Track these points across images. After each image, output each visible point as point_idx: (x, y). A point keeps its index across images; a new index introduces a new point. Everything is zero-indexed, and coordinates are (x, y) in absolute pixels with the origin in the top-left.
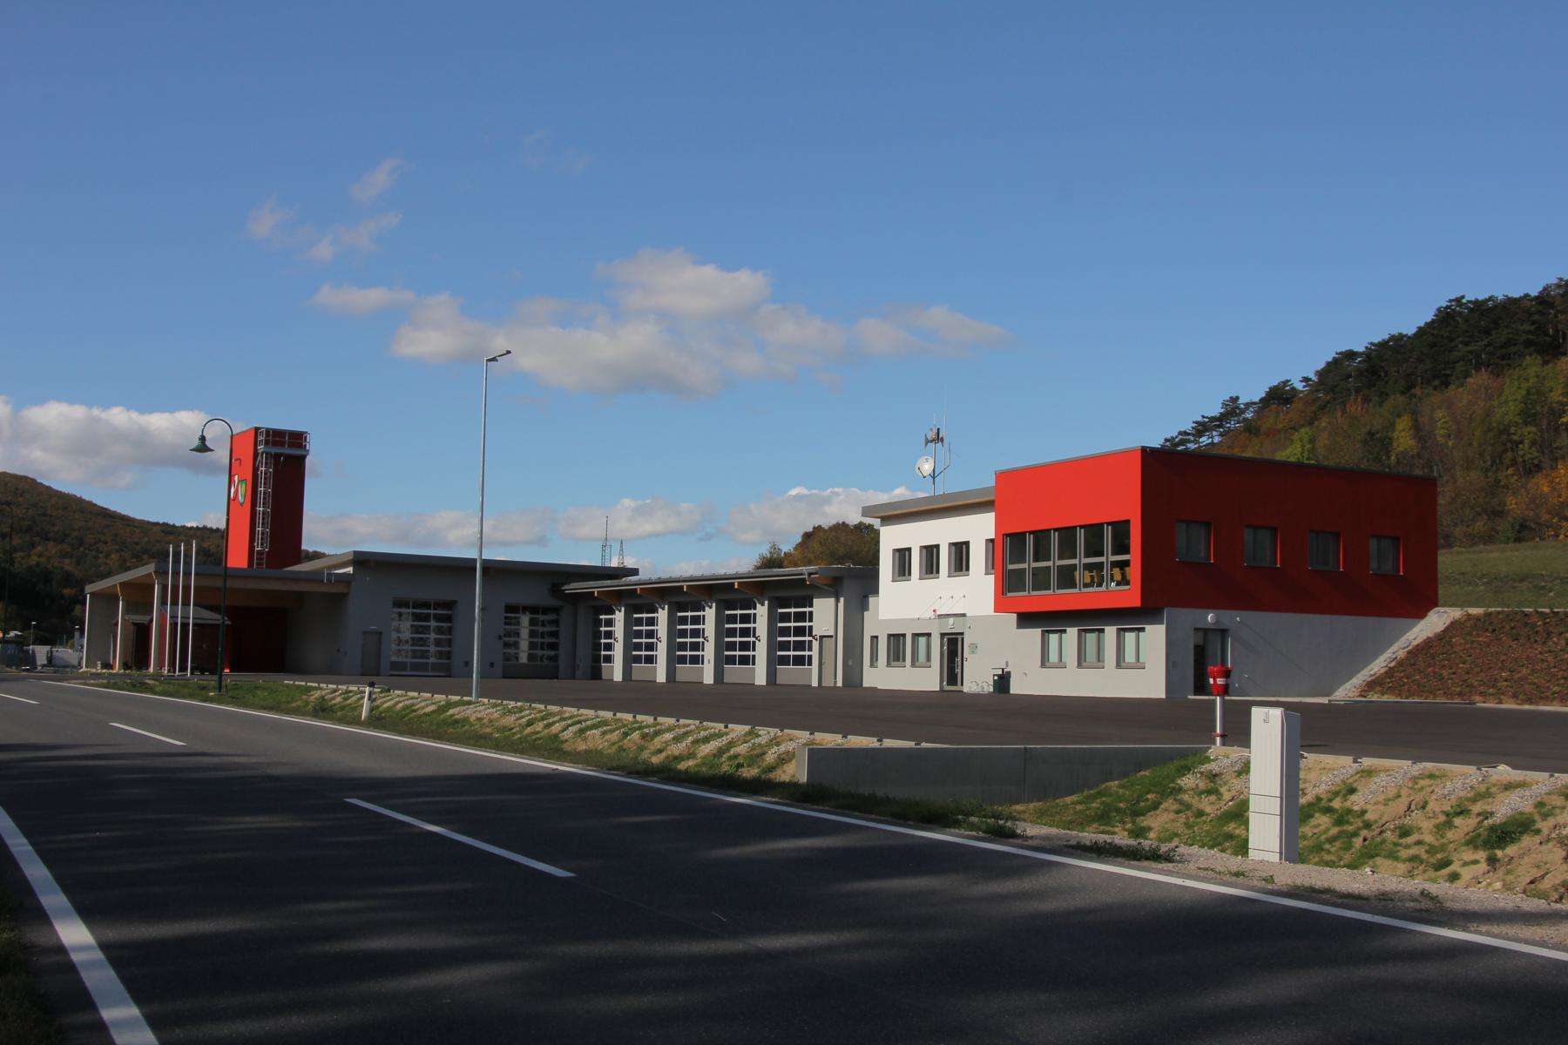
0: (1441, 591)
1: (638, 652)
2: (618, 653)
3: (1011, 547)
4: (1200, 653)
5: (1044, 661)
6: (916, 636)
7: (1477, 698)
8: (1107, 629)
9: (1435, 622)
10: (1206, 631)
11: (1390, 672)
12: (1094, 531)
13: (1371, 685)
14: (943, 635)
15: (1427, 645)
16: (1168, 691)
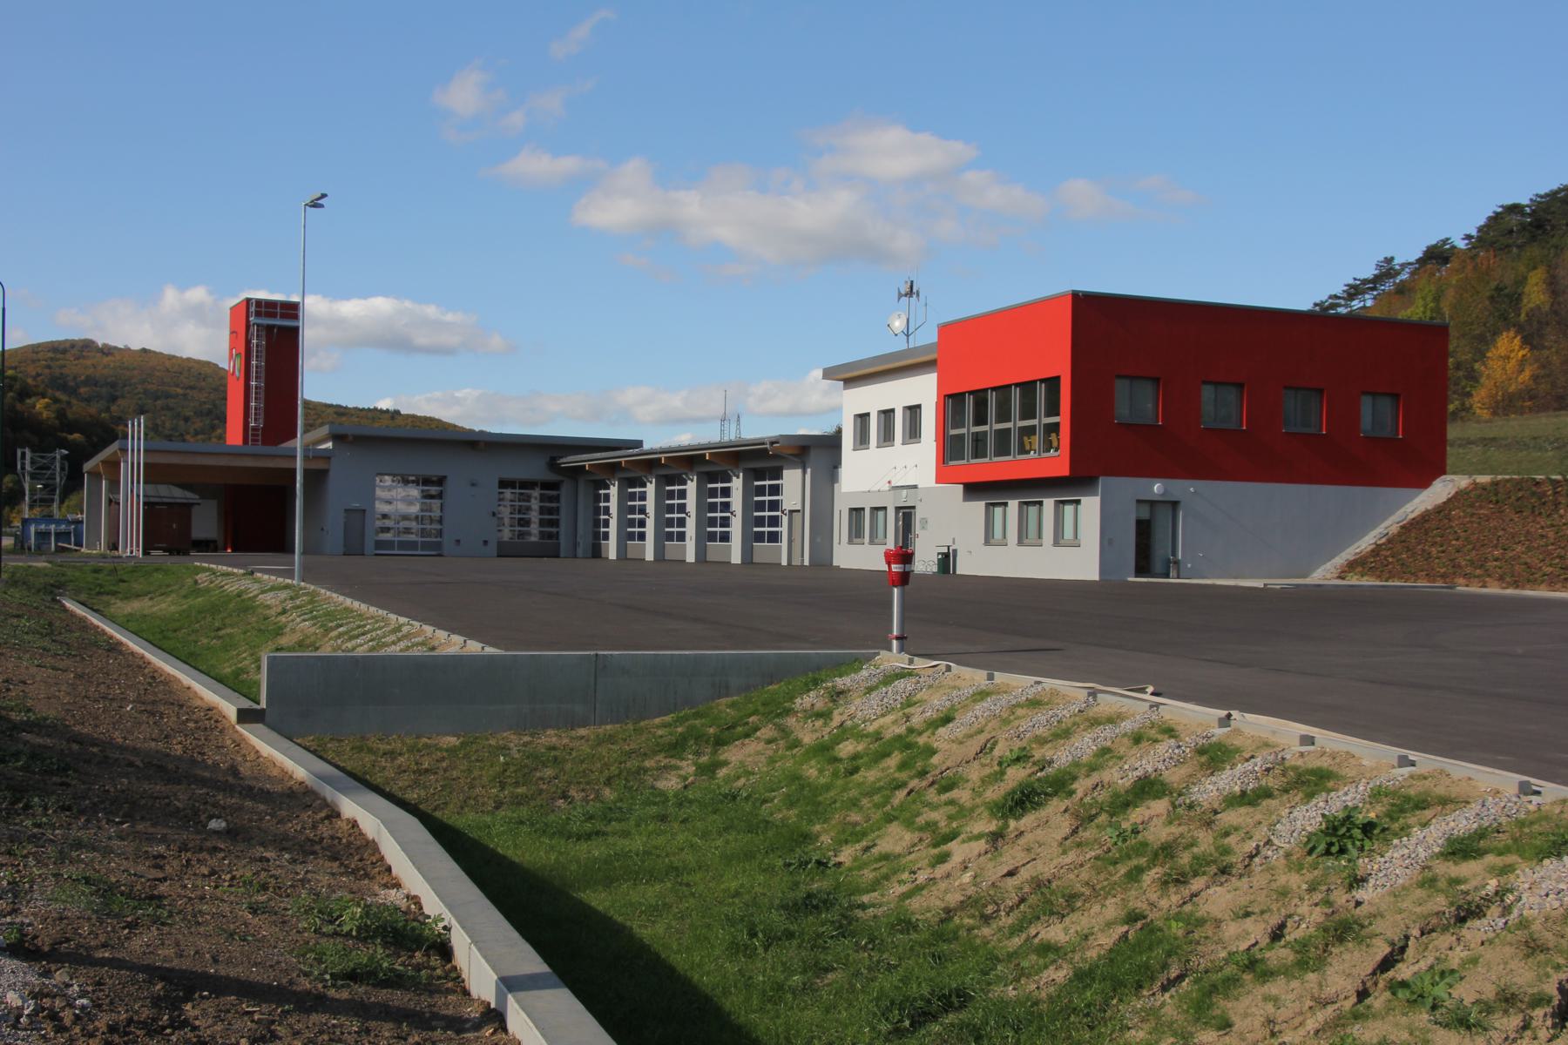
0: (1450, 461)
1: (631, 532)
2: (613, 530)
3: (952, 402)
4: (1144, 530)
5: (988, 539)
7: (1461, 581)
8: (1010, 502)
9: (1440, 491)
10: (1152, 504)
11: (1376, 551)
12: (1028, 387)
13: (1352, 566)
14: (898, 509)
15: (1425, 517)
16: (1102, 572)
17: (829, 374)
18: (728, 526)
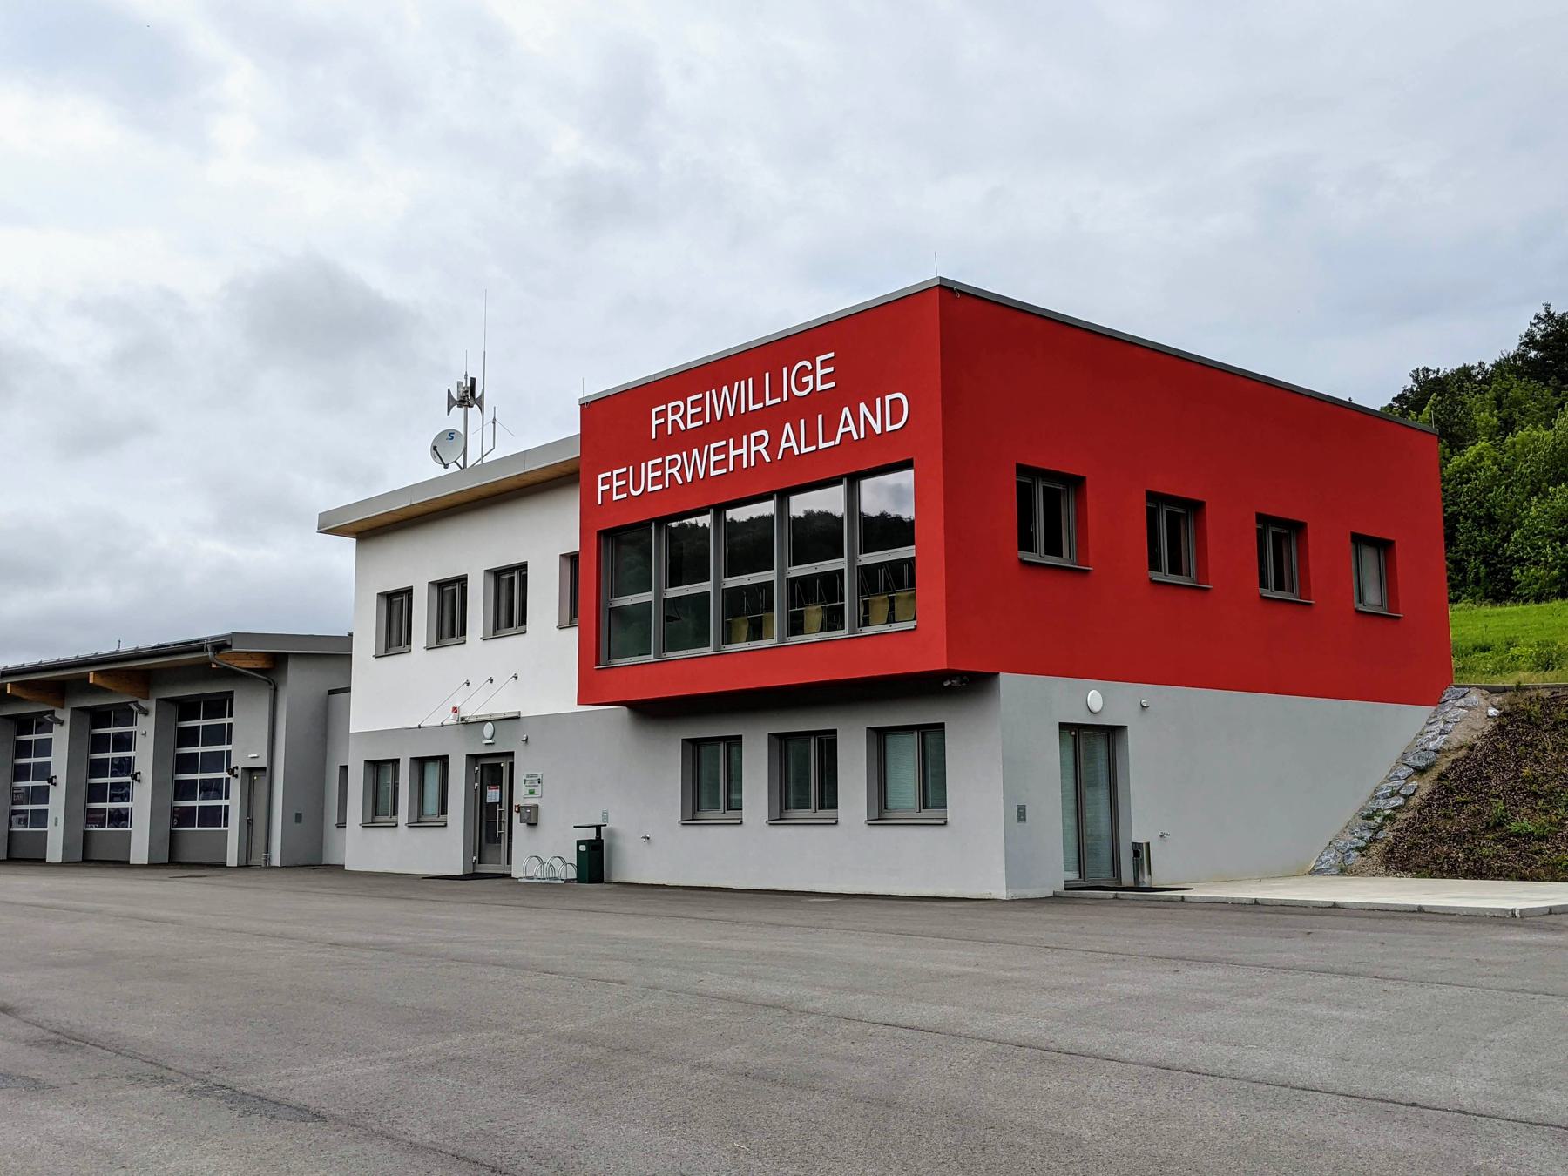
3: (615, 547)
6: (420, 763)
14: (473, 759)
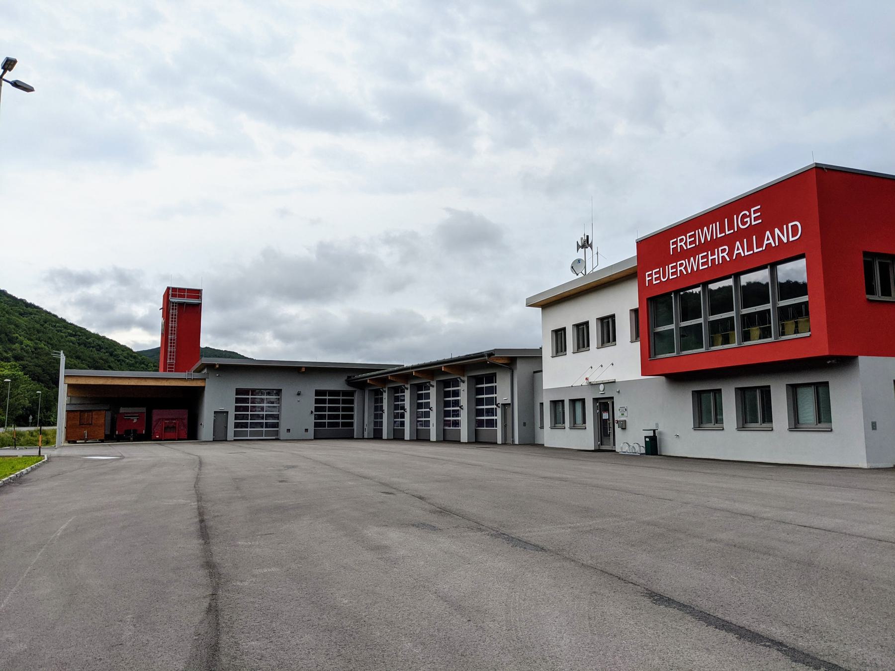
3: (655, 306)
6: (573, 402)
14: (596, 400)
17: (531, 304)
18: (458, 415)
